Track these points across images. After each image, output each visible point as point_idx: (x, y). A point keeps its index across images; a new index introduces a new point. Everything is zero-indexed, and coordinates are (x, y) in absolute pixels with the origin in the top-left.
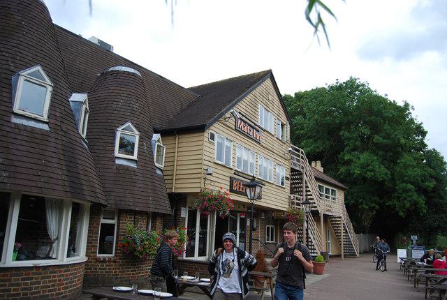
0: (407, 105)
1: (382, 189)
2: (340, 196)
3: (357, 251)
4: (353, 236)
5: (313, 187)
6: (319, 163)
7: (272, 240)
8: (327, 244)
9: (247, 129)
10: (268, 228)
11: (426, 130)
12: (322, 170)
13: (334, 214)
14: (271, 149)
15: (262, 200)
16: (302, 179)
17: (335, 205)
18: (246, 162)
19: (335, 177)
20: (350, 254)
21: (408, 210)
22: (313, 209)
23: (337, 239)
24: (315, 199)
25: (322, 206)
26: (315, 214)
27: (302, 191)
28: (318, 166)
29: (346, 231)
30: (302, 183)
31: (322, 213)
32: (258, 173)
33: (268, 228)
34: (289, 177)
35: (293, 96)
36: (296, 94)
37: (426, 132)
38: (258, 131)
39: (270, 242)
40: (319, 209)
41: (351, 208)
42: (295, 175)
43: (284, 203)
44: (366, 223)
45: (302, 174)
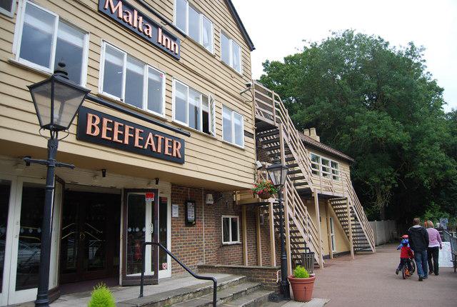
0: (411, 44)
1: (398, 157)
2: (344, 171)
3: (371, 242)
4: (365, 225)
5: (303, 158)
6: (314, 131)
7: (234, 238)
8: (330, 239)
9: (162, 38)
10: (227, 220)
11: (441, 87)
12: (318, 139)
13: (335, 195)
14: (209, 78)
15: (185, 165)
16: (278, 140)
17: (339, 182)
18: (135, 80)
19: (337, 149)
20: (362, 250)
21: (437, 181)
22: (298, 187)
23: (343, 230)
24: (303, 170)
25: (318, 185)
26: (306, 195)
27: (347, 217)
28: (313, 136)
29: (356, 218)
30: (279, 147)
31: (317, 192)
32: (173, 113)
33: (227, 220)
34: (253, 132)
35: (283, 62)
36: (286, 59)
37: (442, 90)
38: (174, 39)
39: (231, 242)
40: (310, 186)
41: (360, 186)
42: (263, 130)
43: (246, 169)
44: (380, 204)
45: (278, 132)
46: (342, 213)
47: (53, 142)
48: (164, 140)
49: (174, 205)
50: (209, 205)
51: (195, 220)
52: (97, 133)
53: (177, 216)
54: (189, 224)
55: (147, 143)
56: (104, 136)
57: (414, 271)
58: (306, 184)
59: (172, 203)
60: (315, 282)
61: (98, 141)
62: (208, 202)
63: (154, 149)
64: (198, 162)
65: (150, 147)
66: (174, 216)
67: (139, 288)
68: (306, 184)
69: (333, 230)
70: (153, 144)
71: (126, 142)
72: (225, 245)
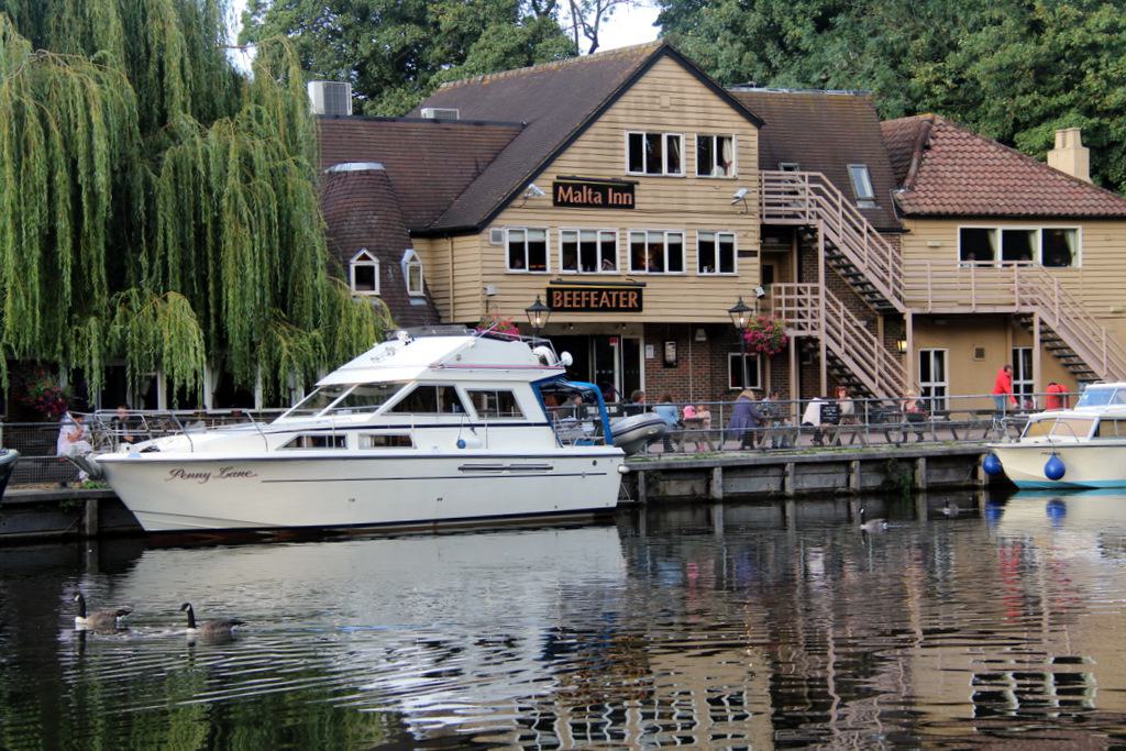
15: (644, 312)
46: (335, 685)
47: (967, 435)
48: (618, 296)
49: (648, 346)
50: (699, 342)
51: (677, 361)
52: (559, 305)
53: (652, 357)
54: (667, 365)
55: (602, 302)
56: (566, 306)
57: (141, 251)
58: (712, 711)
59: (646, 344)
60: (655, 18)
61: (562, 309)
62: (698, 339)
63: (609, 305)
64: (661, 305)
65: (605, 304)
66: (648, 357)
67: (544, 420)
68: (712, 711)
69: (884, 242)
70: (607, 301)
71: (583, 305)
72: (733, 391)
